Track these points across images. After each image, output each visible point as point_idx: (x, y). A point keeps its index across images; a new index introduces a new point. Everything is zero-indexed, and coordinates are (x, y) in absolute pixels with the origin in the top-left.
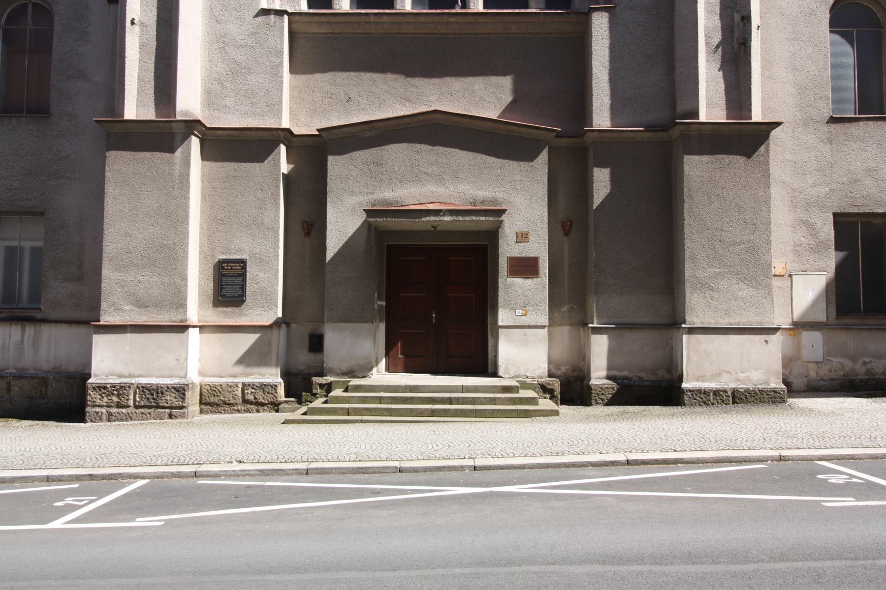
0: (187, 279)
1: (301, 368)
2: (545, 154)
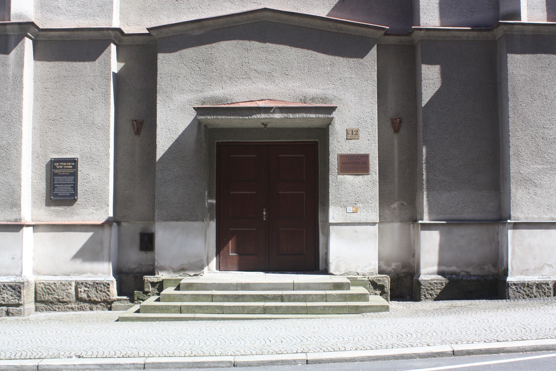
0: (20, 179)
1: (133, 266)
2: (374, 52)
